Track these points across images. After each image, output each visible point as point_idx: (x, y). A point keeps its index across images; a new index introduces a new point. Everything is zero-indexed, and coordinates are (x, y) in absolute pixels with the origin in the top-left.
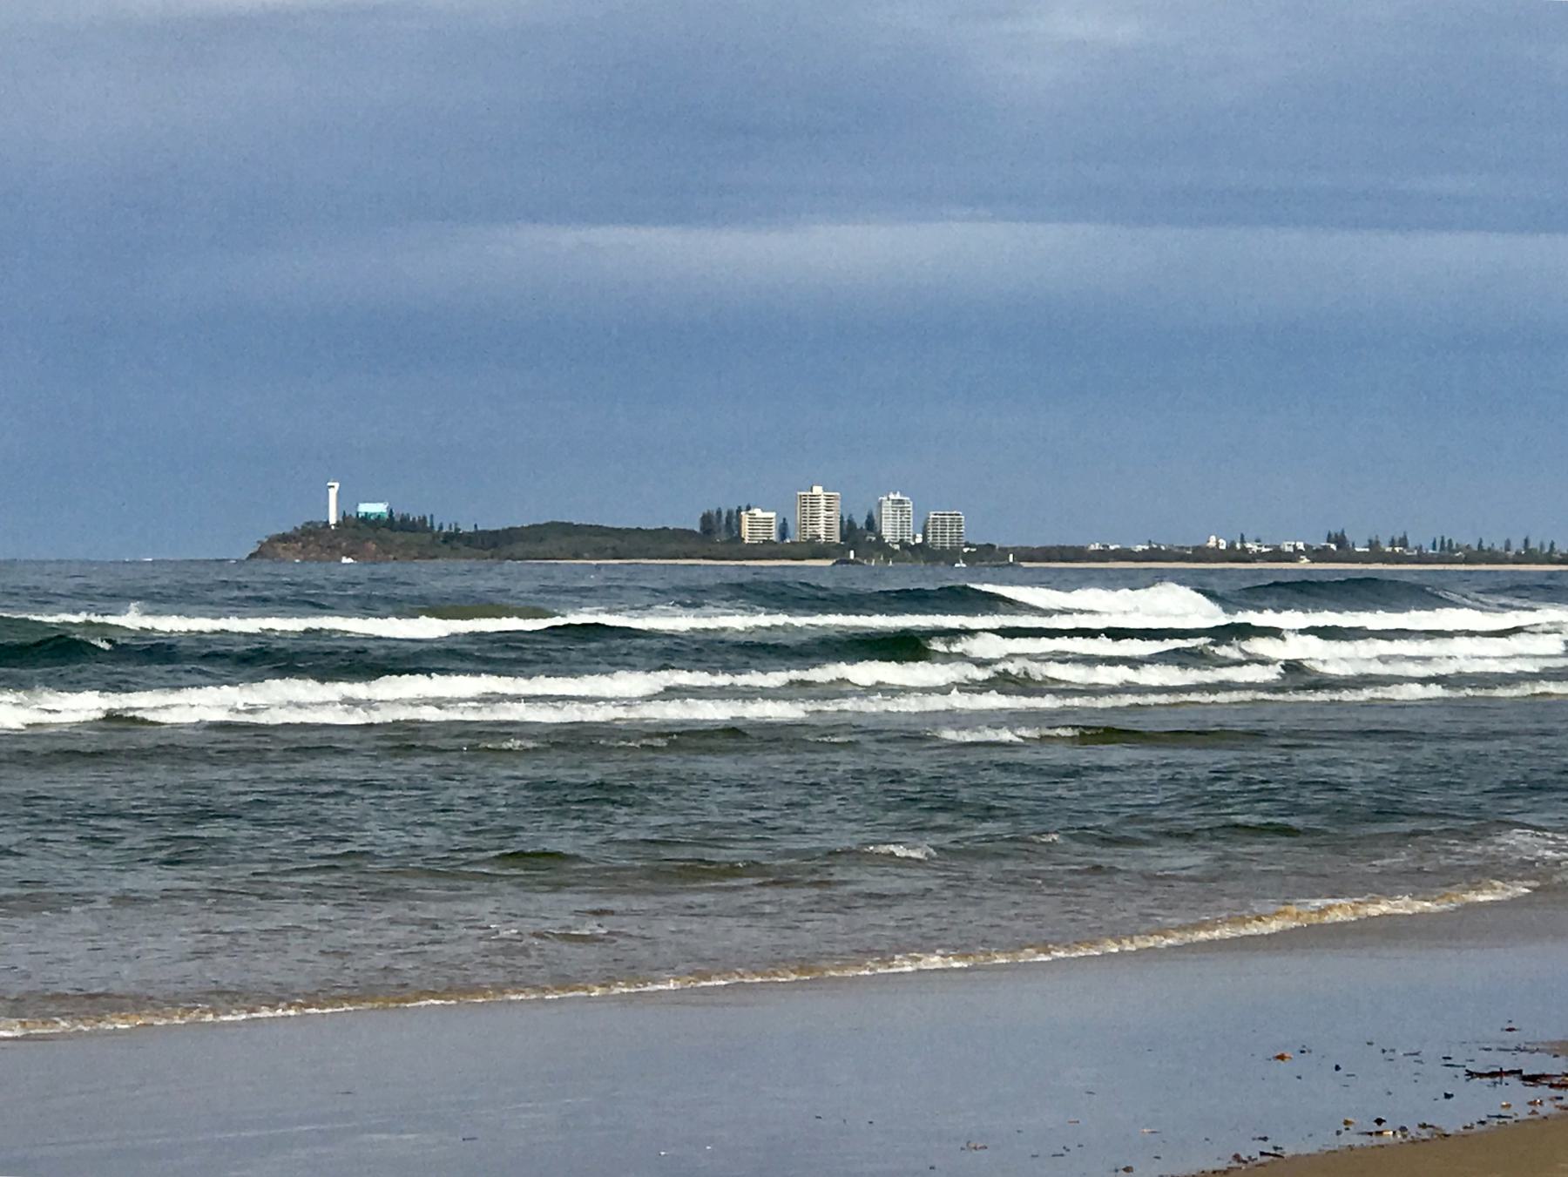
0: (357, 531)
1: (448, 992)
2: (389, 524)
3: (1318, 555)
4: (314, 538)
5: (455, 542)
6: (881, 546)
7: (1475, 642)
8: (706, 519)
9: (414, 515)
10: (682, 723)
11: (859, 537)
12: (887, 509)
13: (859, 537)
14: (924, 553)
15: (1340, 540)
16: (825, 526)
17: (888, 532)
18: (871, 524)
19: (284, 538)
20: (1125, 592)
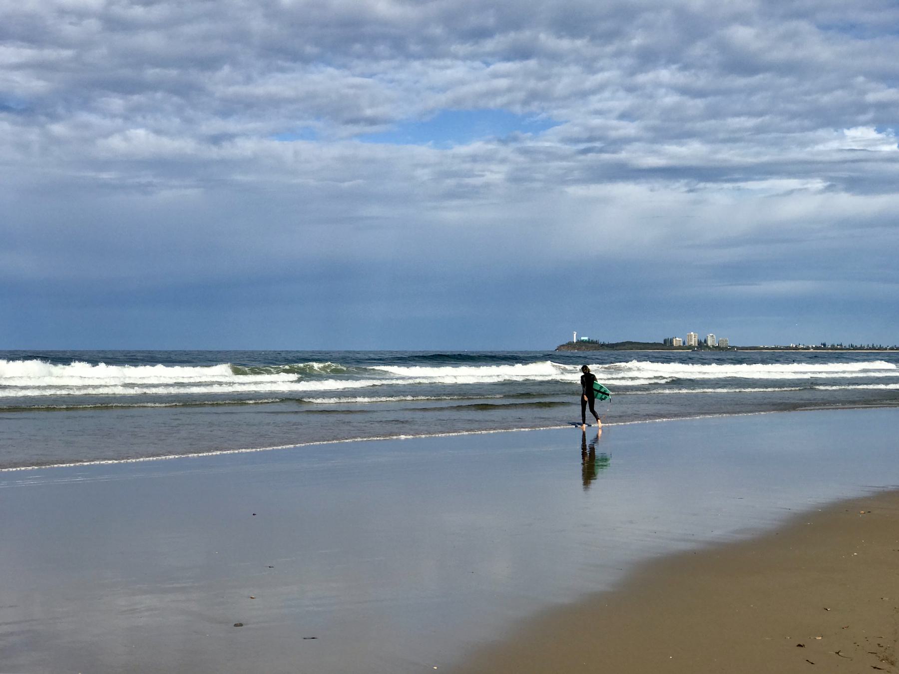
0: (581, 343)
1: (728, 413)
2: (588, 342)
3: (817, 348)
4: (570, 345)
5: (604, 346)
6: (707, 346)
7: (28, 377)
8: (665, 341)
9: (595, 340)
10: (767, 380)
11: (702, 345)
12: (709, 338)
13: (702, 345)
14: (718, 348)
15: (824, 345)
16: (694, 342)
17: (710, 343)
18: (706, 341)
19: (563, 345)
20: (60, 366)
